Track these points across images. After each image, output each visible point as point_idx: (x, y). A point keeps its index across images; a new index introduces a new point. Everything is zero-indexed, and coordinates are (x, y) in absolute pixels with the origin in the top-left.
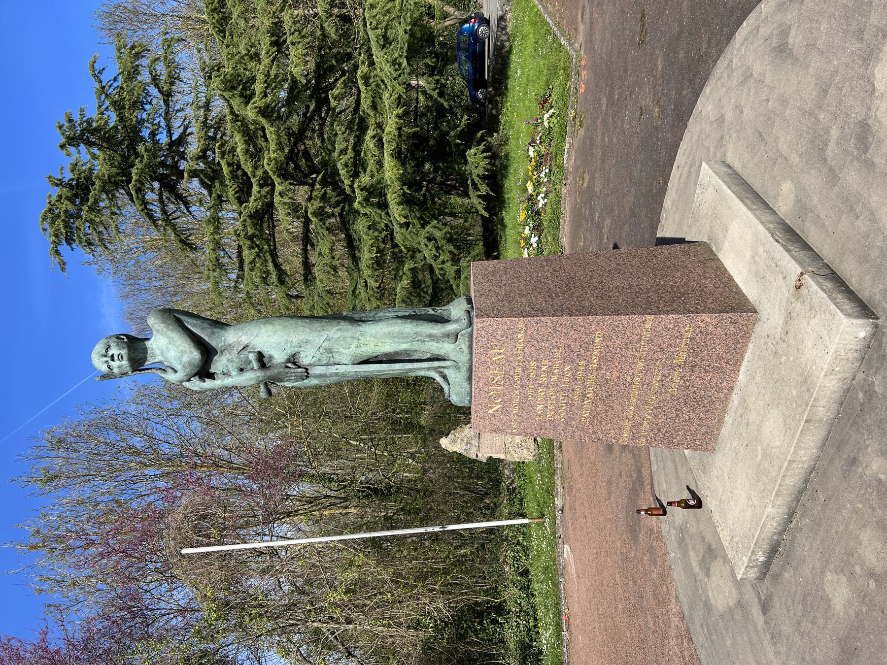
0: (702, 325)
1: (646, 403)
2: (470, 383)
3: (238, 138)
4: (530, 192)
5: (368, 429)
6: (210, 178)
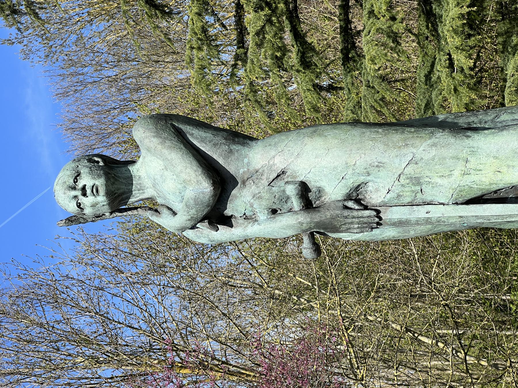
5: (452, 318)
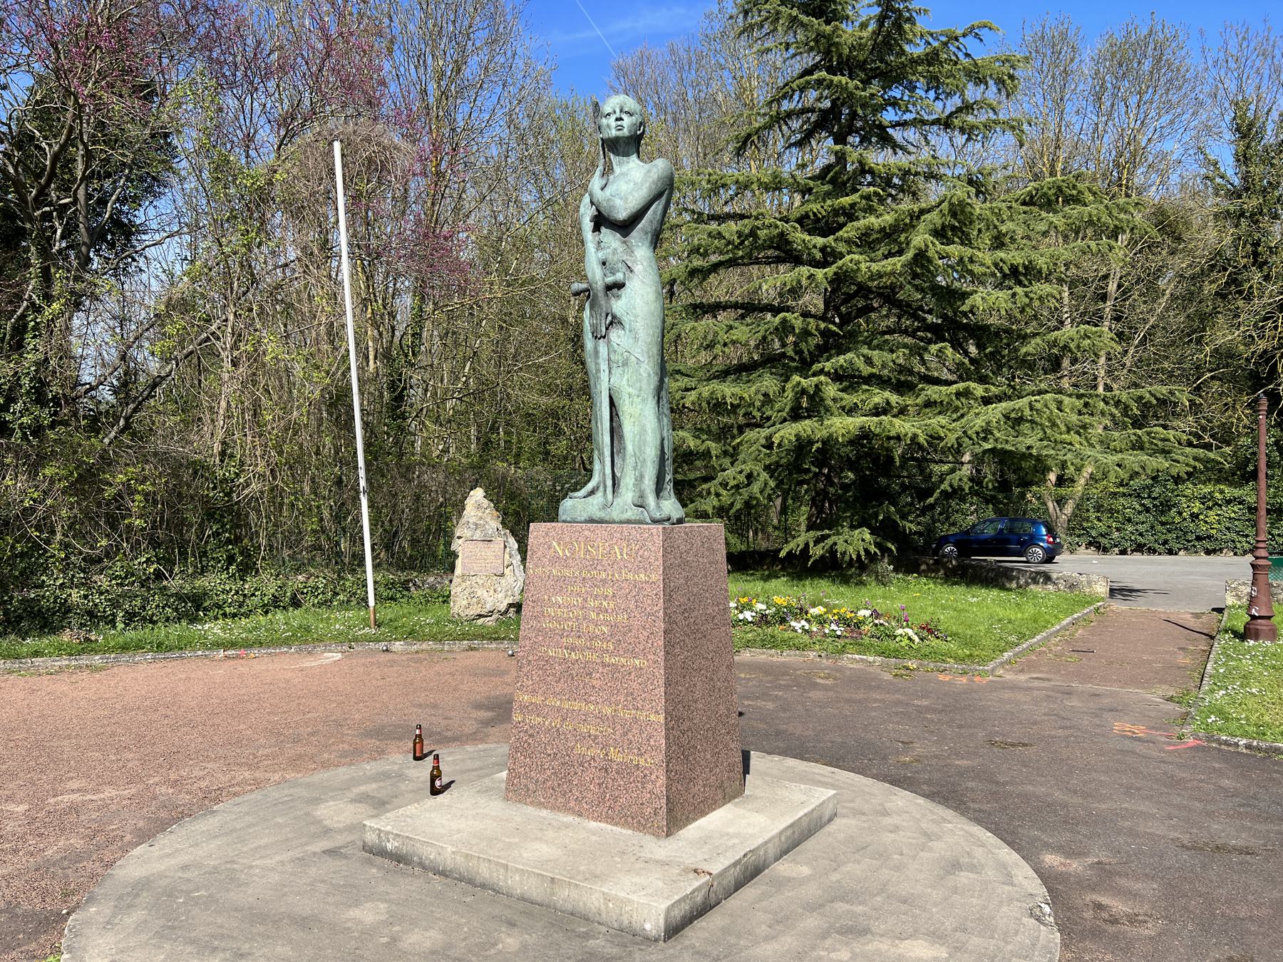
0: (653, 777)
1: (564, 720)
2: (586, 521)
3: (888, 219)
4: (811, 611)
6: (836, 178)
